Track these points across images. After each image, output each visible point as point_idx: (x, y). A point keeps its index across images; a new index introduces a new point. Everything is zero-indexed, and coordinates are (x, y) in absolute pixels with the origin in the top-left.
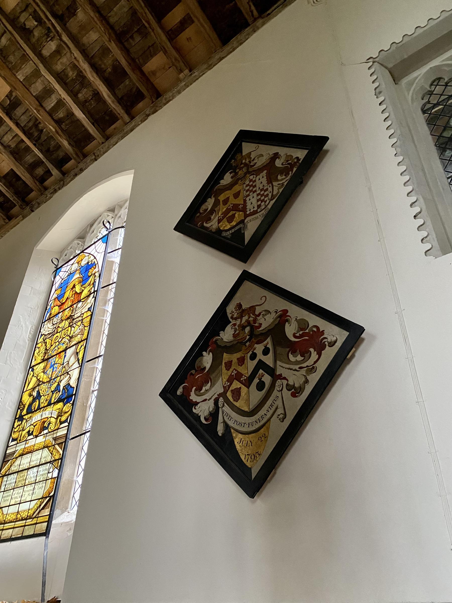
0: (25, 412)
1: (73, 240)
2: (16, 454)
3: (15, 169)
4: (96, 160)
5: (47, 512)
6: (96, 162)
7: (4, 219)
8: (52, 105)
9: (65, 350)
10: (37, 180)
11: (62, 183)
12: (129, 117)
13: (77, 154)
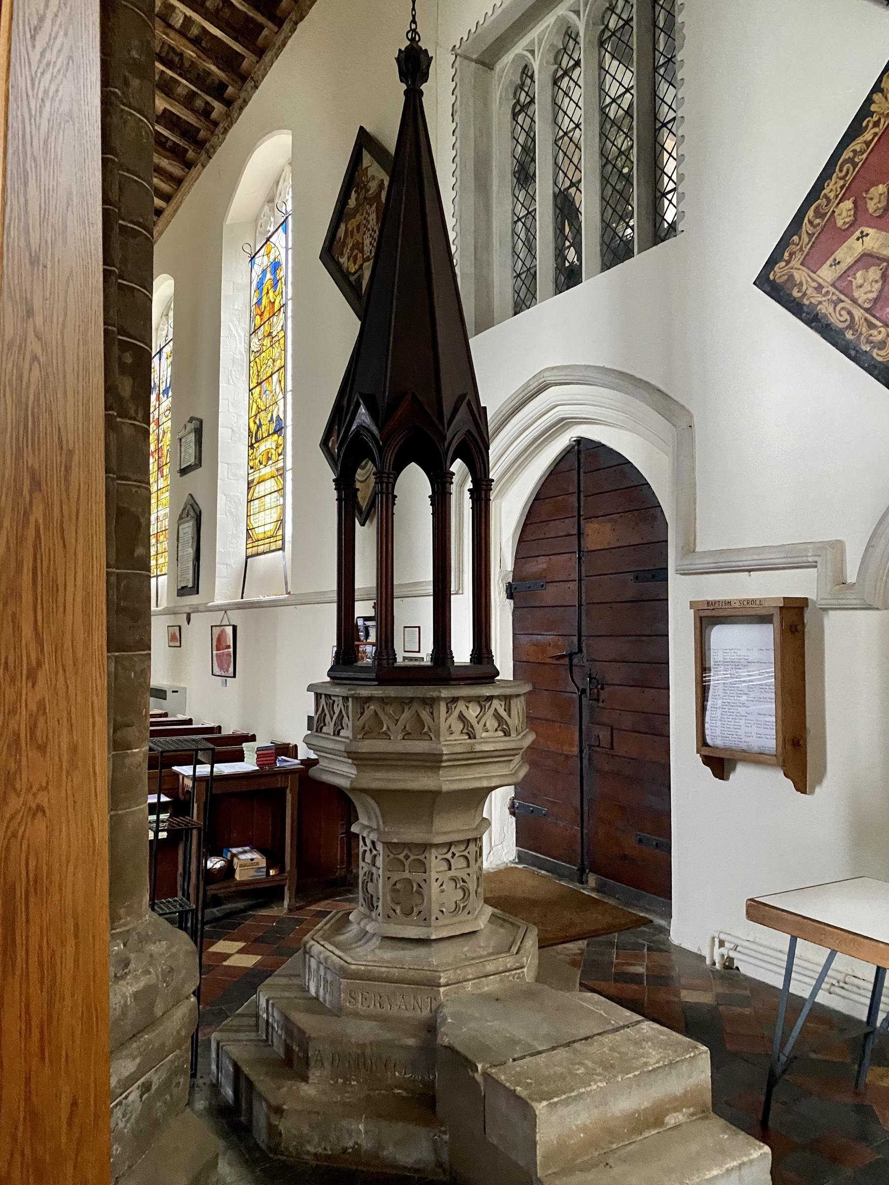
0: (253, 441)
1: (263, 206)
2: (255, 482)
3: (169, 108)
4: (257, 88)
5: (280, 532)
6: (257, 91)
7: (183, 169)
8: (181, 21)
9: (271, 376)
10: (200, 115)
11: (230, 119)
12: (275, 24)
13: (233, 80)
